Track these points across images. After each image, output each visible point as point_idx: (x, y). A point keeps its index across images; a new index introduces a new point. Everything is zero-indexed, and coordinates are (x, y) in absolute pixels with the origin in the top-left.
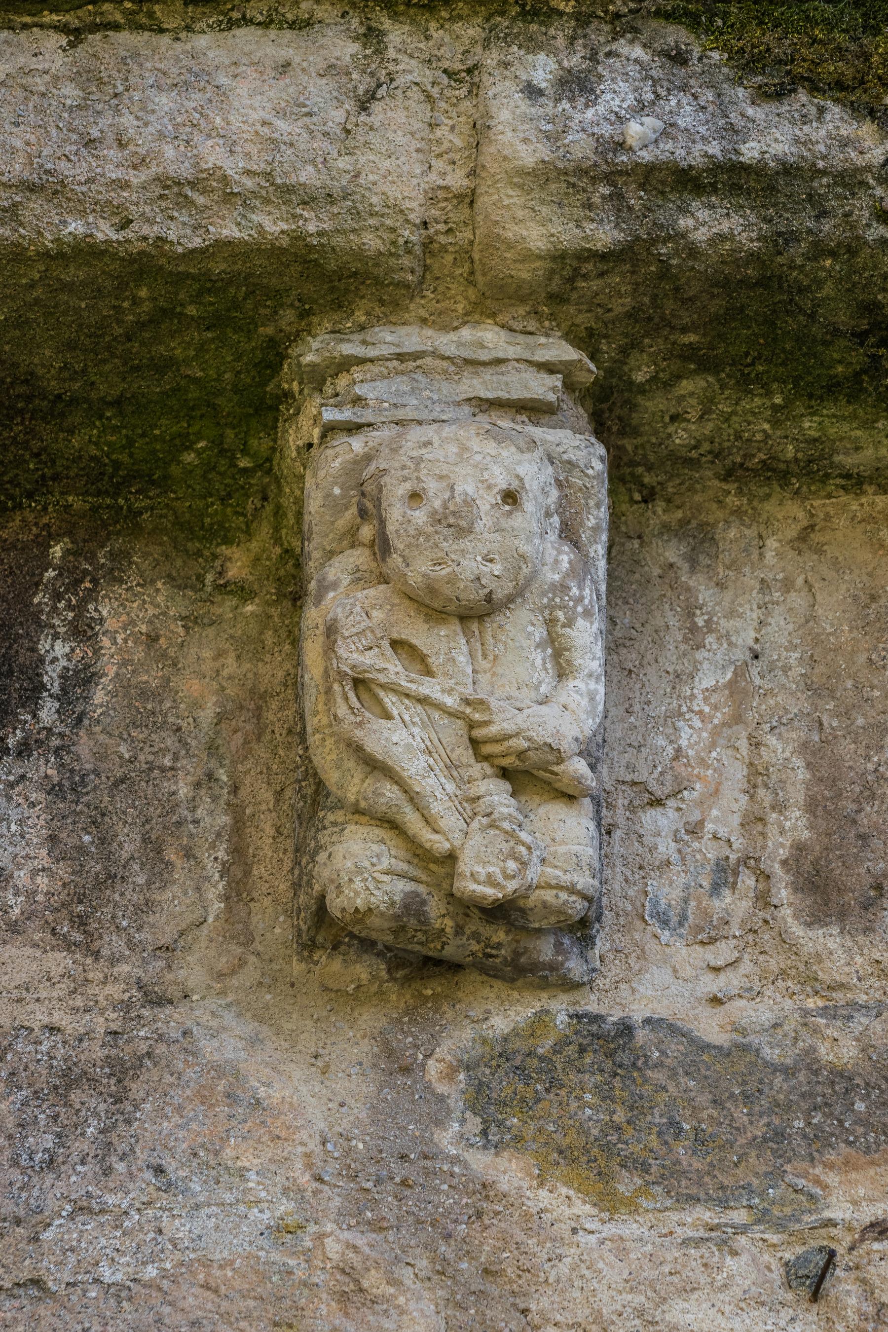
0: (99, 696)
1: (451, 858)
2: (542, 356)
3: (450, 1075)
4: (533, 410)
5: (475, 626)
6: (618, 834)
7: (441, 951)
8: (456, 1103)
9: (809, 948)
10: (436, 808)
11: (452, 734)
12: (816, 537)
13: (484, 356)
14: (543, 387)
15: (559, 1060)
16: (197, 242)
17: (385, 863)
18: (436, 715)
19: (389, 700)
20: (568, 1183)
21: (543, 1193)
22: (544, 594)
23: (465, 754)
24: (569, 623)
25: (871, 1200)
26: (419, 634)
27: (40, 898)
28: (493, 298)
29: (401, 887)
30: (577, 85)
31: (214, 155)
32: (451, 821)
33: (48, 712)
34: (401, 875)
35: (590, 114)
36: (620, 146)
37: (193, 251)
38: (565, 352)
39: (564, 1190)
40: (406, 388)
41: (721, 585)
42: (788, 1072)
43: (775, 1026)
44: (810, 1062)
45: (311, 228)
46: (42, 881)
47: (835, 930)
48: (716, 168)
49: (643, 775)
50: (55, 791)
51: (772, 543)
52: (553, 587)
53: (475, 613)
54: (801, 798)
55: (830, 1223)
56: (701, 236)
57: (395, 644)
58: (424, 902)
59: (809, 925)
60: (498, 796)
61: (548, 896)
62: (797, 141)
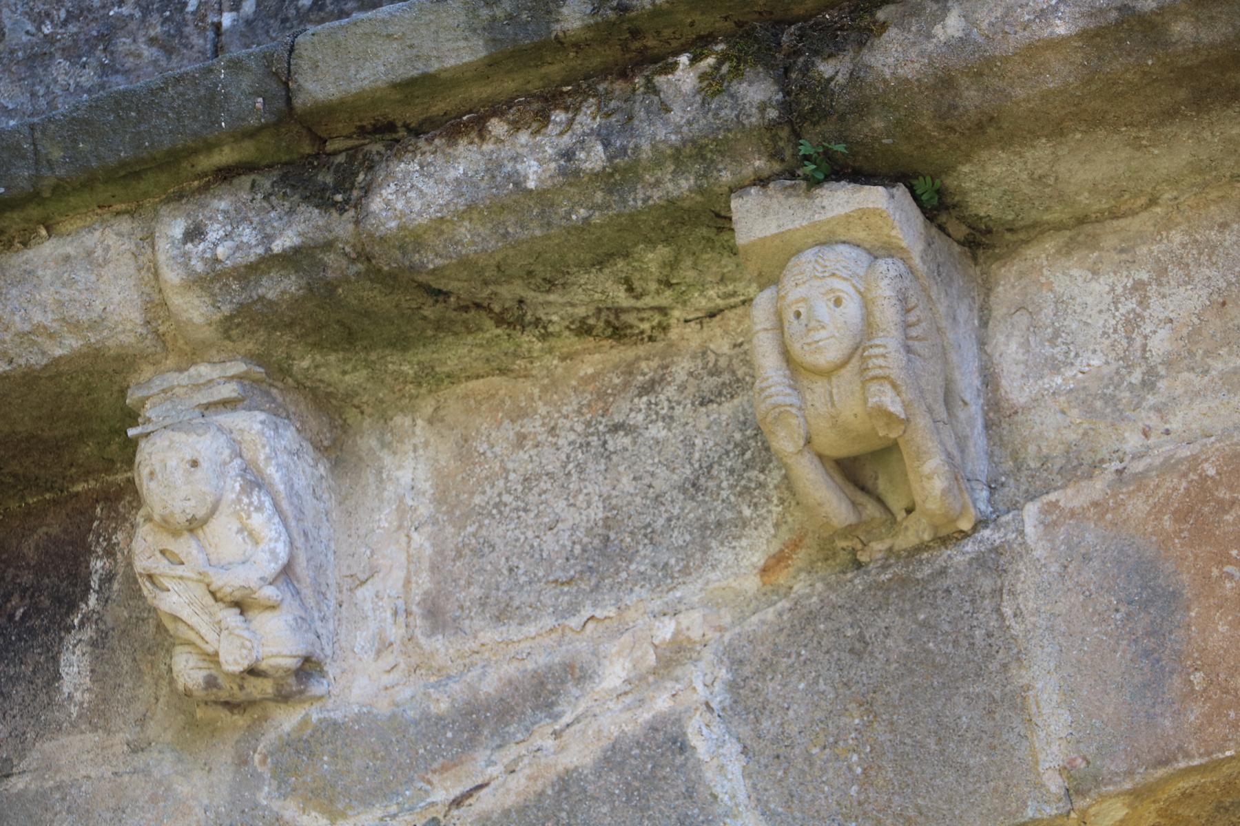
0: (116, 586)
1: (216, 654)
2: (231, 372)
3: (263, 762)
4: (227, 404)
5: (200, 532)
6: (344, 606)
7: (239, 699)
8: (267, 775)
9: (427, 648)
10: (203, 632)
11: (201, 591)
12: (442, 413)
13: (202, 381)
14: (229, 391)
15: (312, 740)
16: (45, 362)
17: (191, 664)
18: (190, 583)
19: (166, 583)
20: (314, 809)
21: (305, 817)
22: (229, 506)
23: (209, 600)
24: (249, 517)
25: (453, 787)
26: (171, 545)
27: (85, 705)
28: (194, 353)
29: (204, 673)
30: (194, 234)
31: (38, 317)
32: (211, 636)
33: (93, 600)
34: (200, 668)
35: (201, 247)
36: (217, 260)
37: (46, 365)
38: (239, 367)
39: (313, 814)
40: (169, 406)
41: (395, 453)
42: (416, 723)
43: (413, 697)
44: (426, 716)
45: (93, 341)
46: (87, 696)
47: (440, 637)
48: (262, 259)
49: (354, 570)
50: (94, 644)
51: (420, 422)
52: (233, 501)
53: (194, 526)
54: (427, 565)
55: (433, 804)
56: (271, 295)
57: (163, 552)
58: (216, 678)
59: (429, 637)
60: (231, 617)
61: (273, 662)
62: (300, 235)
